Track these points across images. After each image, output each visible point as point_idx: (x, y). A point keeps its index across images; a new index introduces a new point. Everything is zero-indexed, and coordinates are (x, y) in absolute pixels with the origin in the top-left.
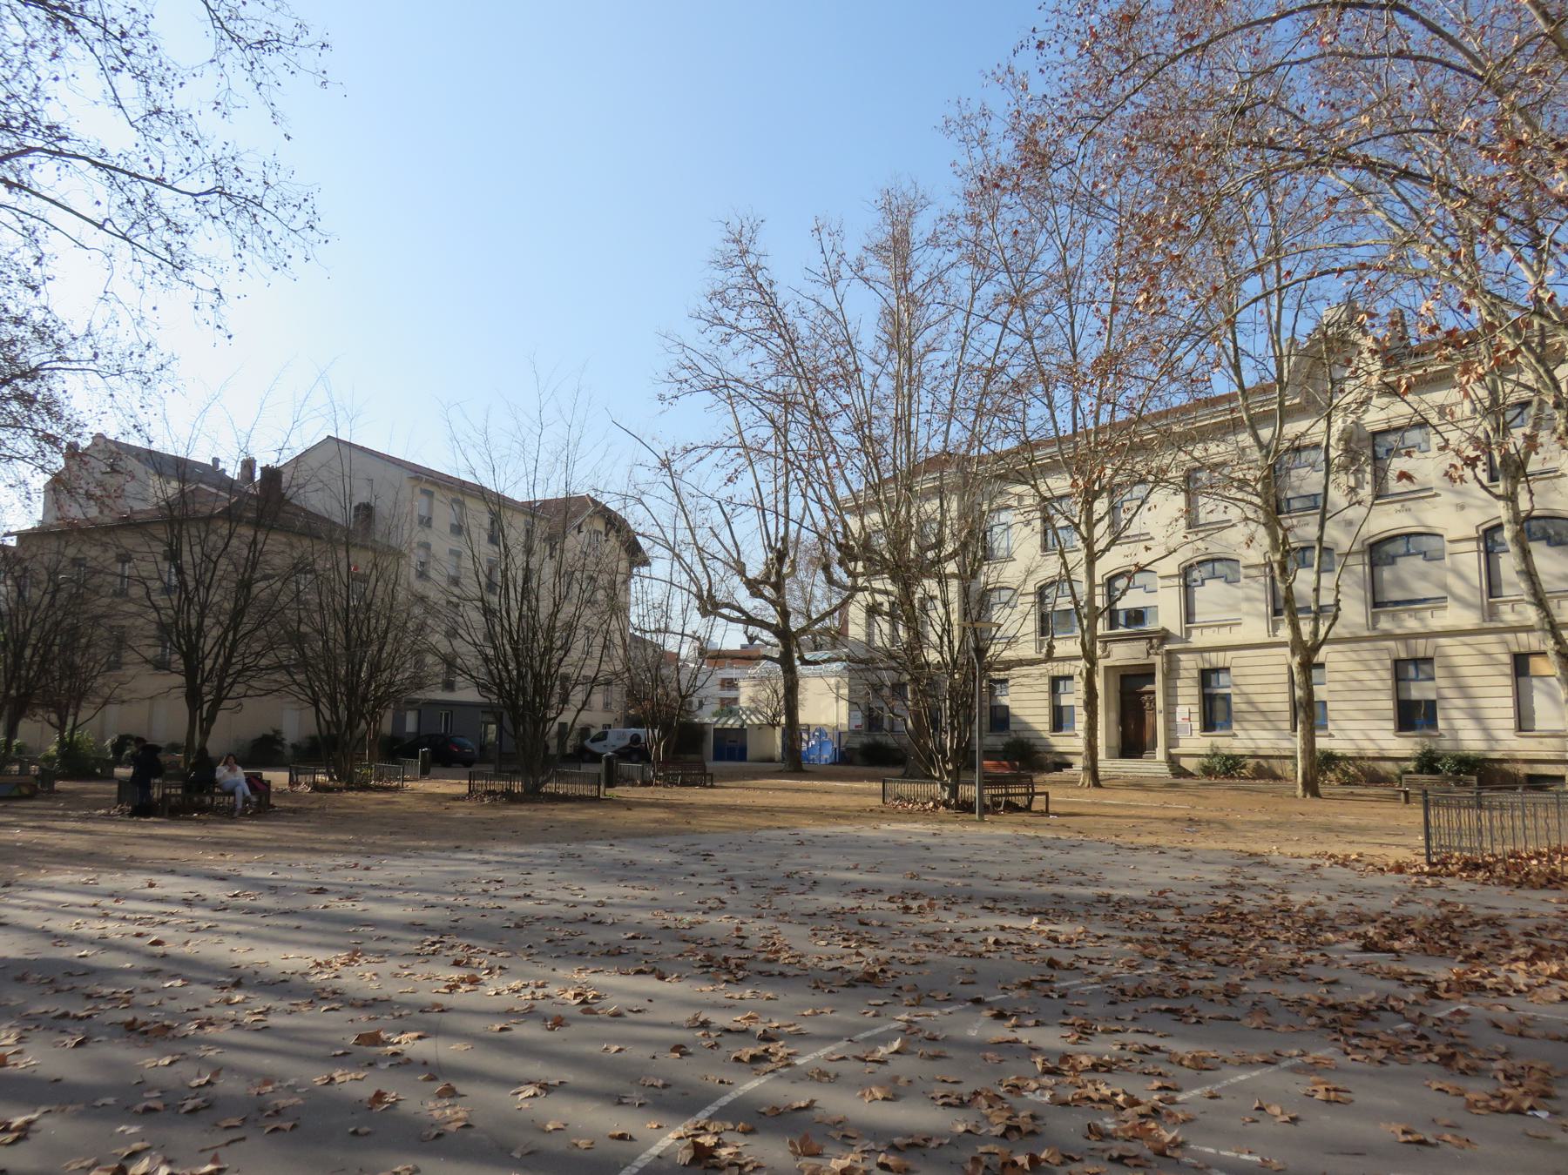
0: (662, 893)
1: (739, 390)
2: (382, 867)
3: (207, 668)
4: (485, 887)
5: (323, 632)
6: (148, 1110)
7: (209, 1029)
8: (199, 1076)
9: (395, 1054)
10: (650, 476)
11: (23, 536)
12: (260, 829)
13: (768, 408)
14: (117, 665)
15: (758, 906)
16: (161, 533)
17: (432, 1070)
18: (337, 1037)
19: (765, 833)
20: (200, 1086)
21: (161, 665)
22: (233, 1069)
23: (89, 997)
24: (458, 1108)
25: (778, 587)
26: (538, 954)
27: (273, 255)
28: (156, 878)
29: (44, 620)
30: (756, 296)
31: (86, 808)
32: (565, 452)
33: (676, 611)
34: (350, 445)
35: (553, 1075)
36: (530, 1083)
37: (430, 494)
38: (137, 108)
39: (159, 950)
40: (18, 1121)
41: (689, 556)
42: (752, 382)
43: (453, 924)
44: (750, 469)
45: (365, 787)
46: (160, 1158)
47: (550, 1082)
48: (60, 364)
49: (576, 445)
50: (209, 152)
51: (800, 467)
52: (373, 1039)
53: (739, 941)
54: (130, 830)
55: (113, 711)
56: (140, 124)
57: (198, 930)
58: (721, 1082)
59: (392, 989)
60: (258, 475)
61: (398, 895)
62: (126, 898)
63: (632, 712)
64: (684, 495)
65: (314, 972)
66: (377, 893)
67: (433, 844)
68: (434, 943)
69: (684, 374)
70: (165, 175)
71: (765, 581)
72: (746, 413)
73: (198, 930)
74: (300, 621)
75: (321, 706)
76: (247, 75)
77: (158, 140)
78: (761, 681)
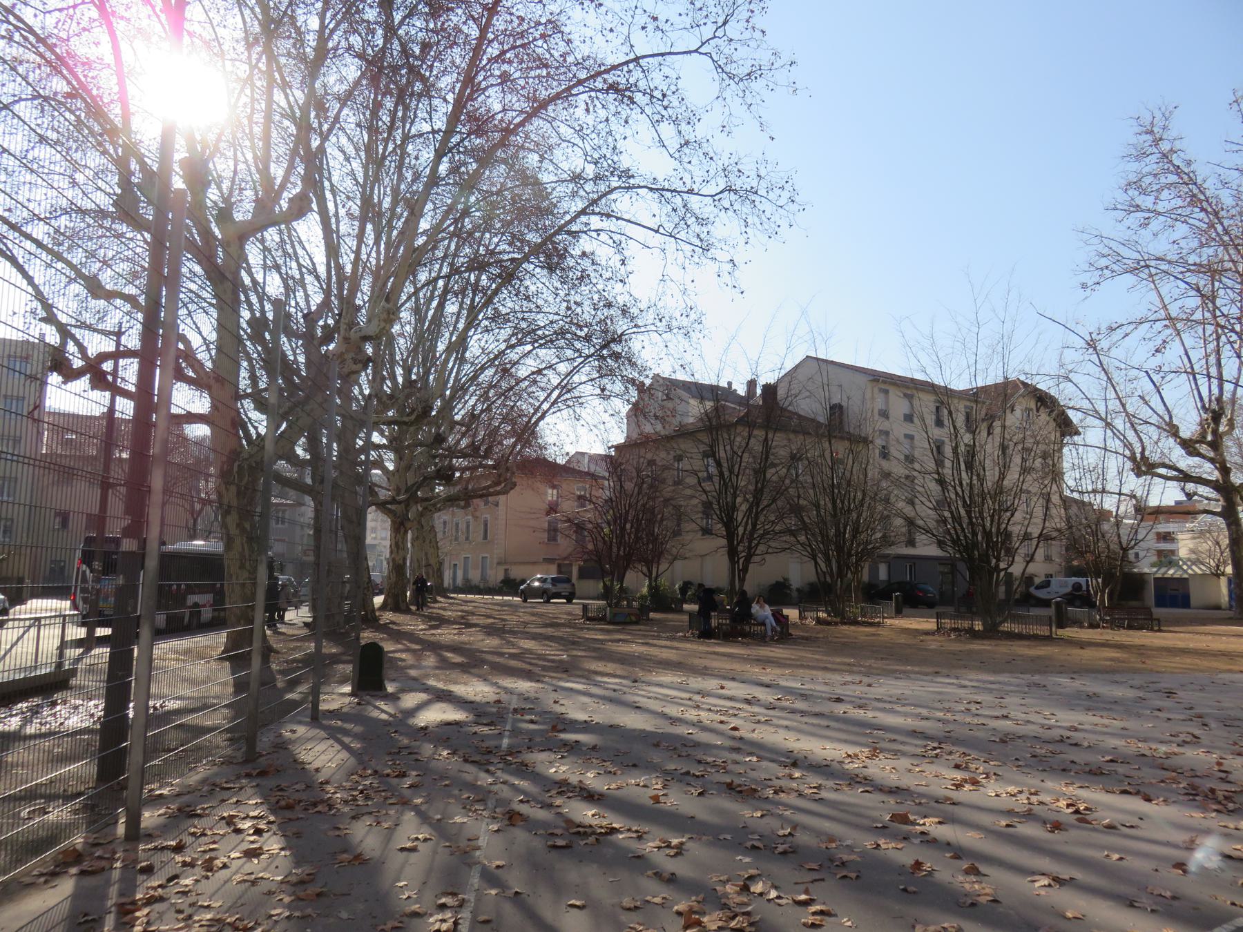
0: (1131, 724)
1: (1163, 267)
2: (881, 685)
3: (740, 533)
4: (968, 706)
5: (817, 505)
6: (754, 847)
7: (782, 795)
8: (782, 828)
9: (923, 833)
10: (1077, 356)
11: (618, 448)
12: (786, 651)
13: (1192, 279)
14: (677, 533)
15: (1236, 744)
16: (705, 438)
17: (959, 853)
18: (876, 814)
19: (1227, 677)
20: (784, 836)
21: (706, 531)
22: (805, 828)
23: (700, 762)
24: (984, 885)
25: (1216, 445)
26: (1026, 766)
27: (767, 227)
28: (724, 683)
29: (637, 503)
30: (1173, 178)
31: (671, 632)
32: (1000, 345)
33: (1112, 472)
34: (826, 361)
35: (1066, 872)
36: (1043, 874)
37: (886, 392)
38: (673, 144)
39: (736, 733)
40: (675, 841)
41: (1119, 423)
42: (1175, 258)
43: (947, 734)
44: (1177, 339)
45: (855, 623)
46: (770, 883)
47: (1061, 877)
48: (635, 330)
49: (1010, 338)
50: (720, 163)
51: (1233, 330)
52: (903, 819)
53: (1223, 775)
54: (702, 648)
55: (678, 564)
56: (677, 155)
57: (759, 722)
58: (1233, 904)
59: (907, 781)
60: (759, 391)
61: (898, 708)
62: (708, 695)
63: (1075, 563)
64: (1111, 370)
65: (847, 761)
66: (881, 705)
67: (917, 669)
68: (935, 749)
69: (1103, 262)
70: (694, 186)
71: (1202, 439)
72: (1170, 288)
73: (759, 722)
74: (799, 497)
75: (818, 560)
76: (741, 100)
77: (690, 162)
78: (1201, 534)
